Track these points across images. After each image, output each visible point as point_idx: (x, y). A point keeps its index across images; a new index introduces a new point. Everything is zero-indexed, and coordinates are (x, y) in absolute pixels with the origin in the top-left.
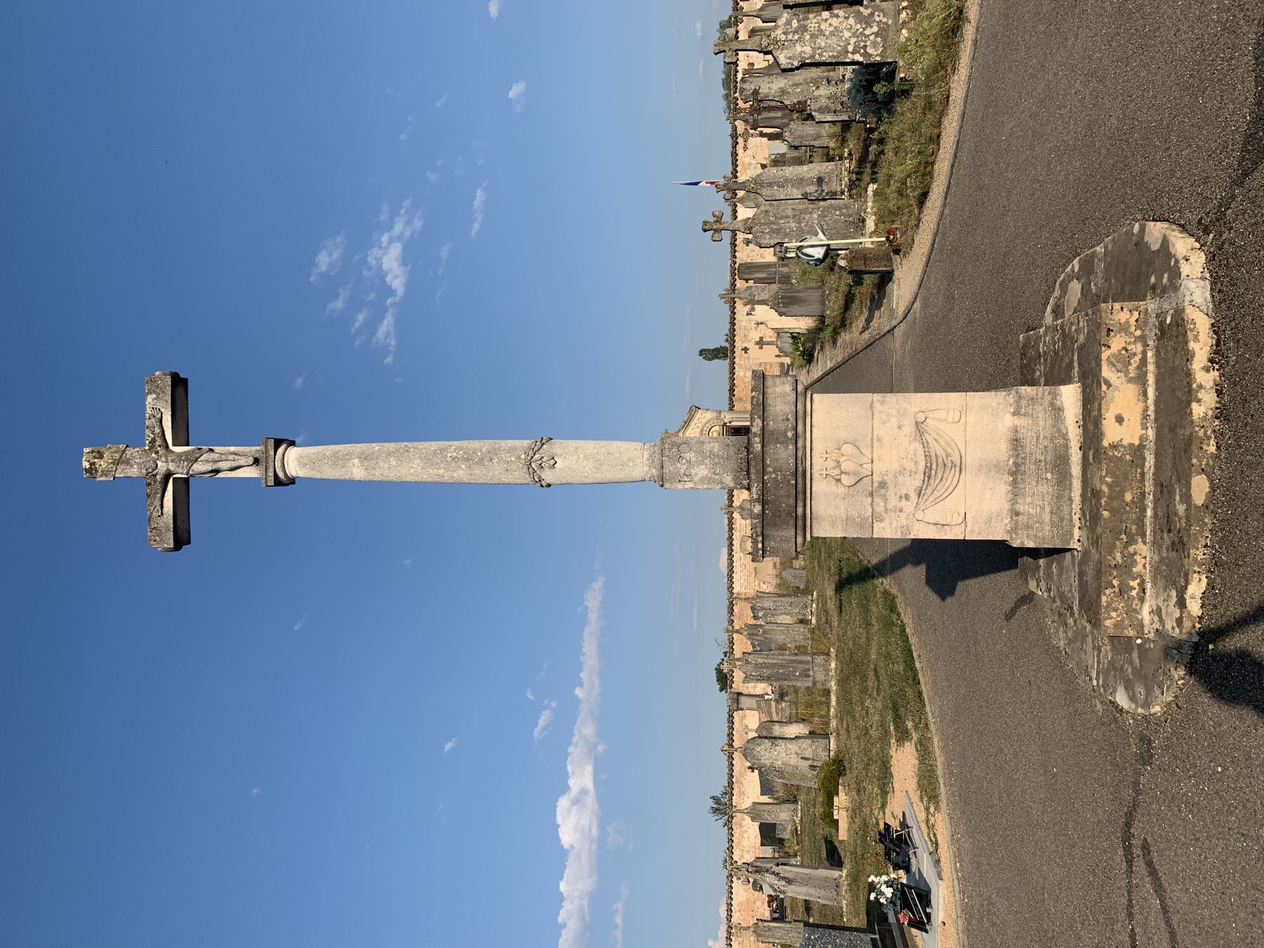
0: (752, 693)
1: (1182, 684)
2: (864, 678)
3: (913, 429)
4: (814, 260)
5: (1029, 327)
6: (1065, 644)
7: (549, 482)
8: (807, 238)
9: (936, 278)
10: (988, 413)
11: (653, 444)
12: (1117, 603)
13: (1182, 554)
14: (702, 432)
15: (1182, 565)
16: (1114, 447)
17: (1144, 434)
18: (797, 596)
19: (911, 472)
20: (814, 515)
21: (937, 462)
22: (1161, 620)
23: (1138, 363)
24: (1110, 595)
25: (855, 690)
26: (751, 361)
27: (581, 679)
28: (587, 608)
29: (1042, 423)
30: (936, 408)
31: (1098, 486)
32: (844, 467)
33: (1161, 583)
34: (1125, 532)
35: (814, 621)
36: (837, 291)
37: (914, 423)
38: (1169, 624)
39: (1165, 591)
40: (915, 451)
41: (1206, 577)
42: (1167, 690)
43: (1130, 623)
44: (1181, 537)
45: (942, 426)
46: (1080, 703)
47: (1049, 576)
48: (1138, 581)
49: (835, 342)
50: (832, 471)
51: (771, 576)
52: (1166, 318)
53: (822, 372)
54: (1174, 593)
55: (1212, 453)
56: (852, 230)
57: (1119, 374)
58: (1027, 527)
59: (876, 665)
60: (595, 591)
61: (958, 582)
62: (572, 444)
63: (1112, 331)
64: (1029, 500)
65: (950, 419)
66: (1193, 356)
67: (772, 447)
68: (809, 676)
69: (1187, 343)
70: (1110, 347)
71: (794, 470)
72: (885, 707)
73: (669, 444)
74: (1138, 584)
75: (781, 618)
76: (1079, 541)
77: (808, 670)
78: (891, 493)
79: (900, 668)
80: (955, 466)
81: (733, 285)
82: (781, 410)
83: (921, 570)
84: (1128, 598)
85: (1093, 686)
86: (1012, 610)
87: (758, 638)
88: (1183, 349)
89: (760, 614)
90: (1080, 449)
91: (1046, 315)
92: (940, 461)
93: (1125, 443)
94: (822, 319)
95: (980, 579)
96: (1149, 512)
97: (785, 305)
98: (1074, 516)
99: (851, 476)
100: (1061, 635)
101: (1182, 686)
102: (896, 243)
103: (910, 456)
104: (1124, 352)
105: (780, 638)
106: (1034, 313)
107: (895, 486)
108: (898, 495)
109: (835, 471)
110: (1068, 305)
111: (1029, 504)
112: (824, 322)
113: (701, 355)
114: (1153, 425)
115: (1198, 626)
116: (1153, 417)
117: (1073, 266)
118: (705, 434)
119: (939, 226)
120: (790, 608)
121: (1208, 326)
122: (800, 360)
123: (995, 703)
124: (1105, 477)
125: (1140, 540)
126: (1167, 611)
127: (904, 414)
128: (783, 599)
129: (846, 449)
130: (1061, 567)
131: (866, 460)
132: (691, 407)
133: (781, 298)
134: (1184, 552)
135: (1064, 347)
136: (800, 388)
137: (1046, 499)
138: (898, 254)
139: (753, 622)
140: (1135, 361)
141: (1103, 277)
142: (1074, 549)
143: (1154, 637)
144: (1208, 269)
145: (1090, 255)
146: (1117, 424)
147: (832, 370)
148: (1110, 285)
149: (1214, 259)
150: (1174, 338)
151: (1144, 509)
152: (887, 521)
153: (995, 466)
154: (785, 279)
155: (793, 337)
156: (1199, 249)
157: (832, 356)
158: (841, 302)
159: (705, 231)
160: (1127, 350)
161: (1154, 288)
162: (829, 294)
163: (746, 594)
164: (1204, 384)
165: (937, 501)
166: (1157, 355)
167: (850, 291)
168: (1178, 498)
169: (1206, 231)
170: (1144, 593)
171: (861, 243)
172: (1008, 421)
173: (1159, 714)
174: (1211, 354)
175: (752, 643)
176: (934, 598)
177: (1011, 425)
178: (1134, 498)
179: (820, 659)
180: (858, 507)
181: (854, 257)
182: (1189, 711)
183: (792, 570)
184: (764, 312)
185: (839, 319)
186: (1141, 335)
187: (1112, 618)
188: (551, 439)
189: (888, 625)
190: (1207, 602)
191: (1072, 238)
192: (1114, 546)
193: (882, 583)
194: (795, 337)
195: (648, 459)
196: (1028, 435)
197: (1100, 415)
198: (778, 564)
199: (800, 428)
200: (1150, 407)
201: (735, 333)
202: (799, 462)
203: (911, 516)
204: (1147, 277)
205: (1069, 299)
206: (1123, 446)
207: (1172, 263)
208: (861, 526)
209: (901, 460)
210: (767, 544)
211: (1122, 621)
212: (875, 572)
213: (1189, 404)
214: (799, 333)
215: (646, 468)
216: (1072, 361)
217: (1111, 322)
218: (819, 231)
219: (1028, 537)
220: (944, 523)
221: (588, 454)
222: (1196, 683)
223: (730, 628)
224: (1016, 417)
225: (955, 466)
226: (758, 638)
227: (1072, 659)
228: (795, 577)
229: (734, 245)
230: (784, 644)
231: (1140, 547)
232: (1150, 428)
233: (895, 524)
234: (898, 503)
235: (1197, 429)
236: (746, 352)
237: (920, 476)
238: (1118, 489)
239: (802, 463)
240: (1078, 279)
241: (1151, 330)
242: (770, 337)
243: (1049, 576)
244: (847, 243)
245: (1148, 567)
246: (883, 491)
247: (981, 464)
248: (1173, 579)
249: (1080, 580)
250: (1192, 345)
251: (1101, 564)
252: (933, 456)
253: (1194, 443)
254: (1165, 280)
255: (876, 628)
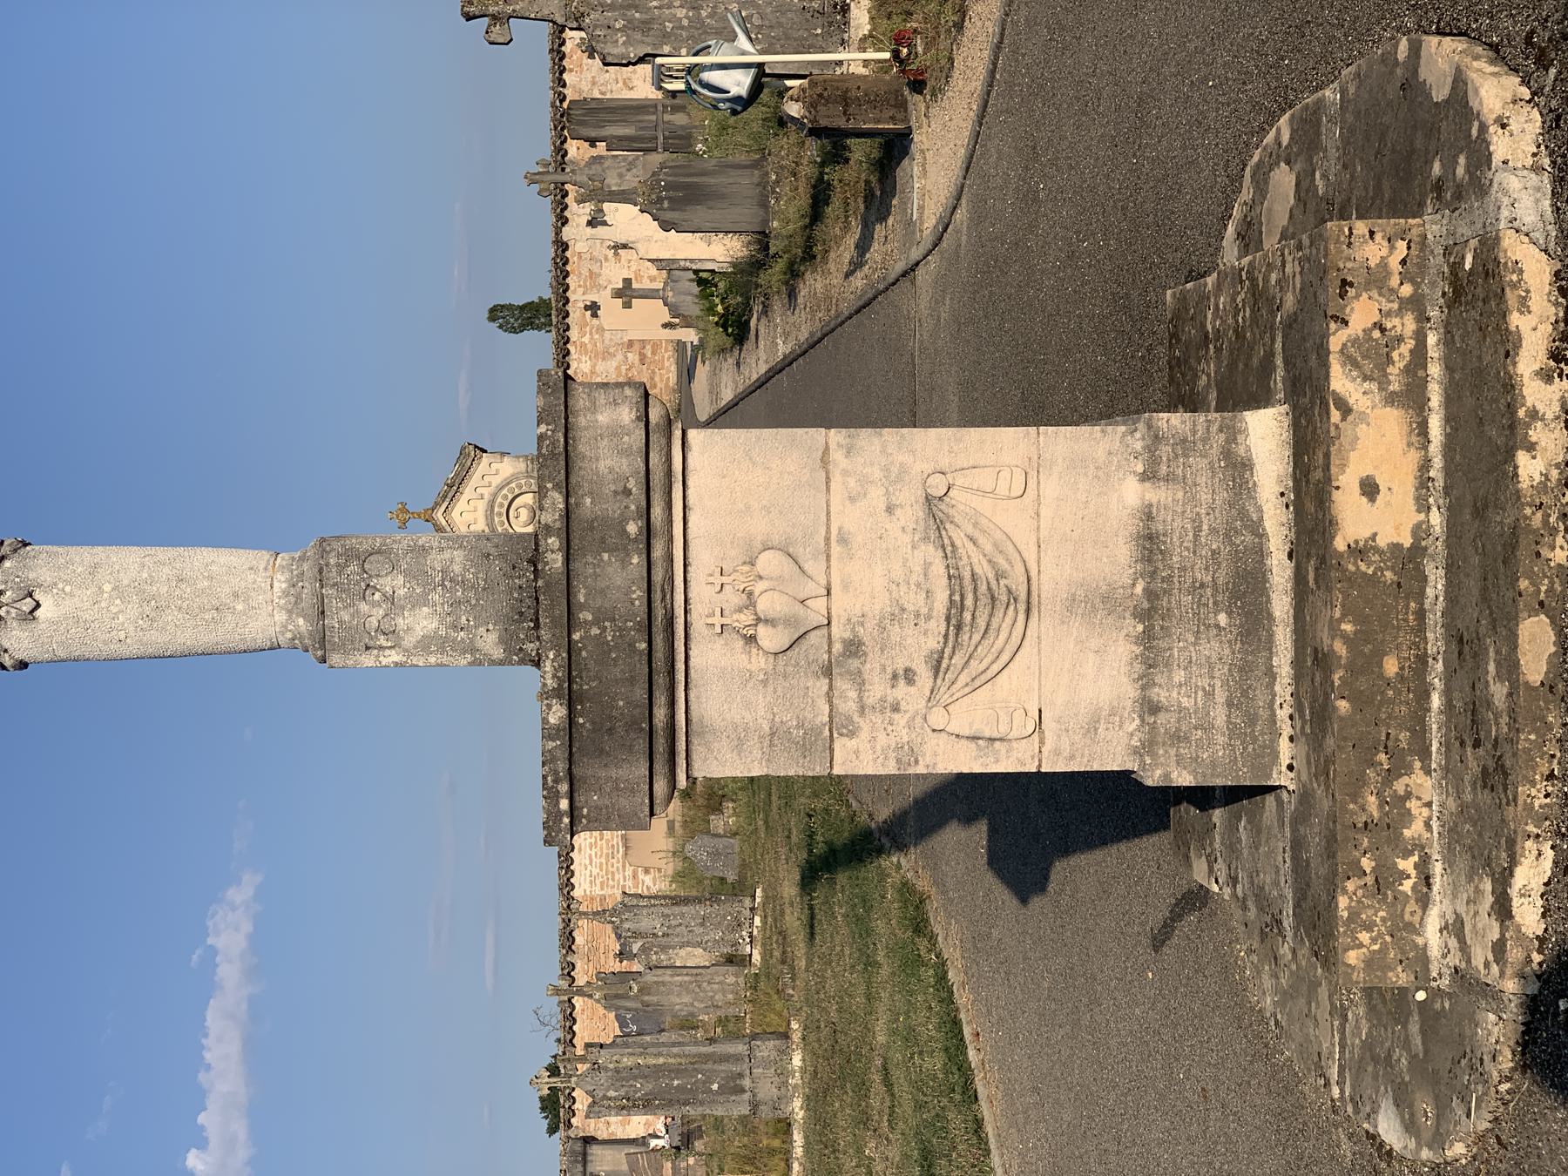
0: (620, 1135)
1: (1508, 1092)
2: (863, 1089)
3: (921, 514)
4: (729, 100)
5: (1191, 271)
6: (1275, 1003)
7: (20, 656)
8: (710, 47)
9: (999, 152)
10: (1086, 474)
11: (297, 555)
12: (1370, 912)
13: (1502, 796)
14: (492, 507)
15: (1503, 821)
16: (1359, 551)
17: (1423, 522)
18: (718, 901)
19: (918, 615)
20: (694, 727)
21: (975, 590)
22: (1464, 948)
23: (1408, 359)
24: (1355, 894)
25: (844, 1117)
26: (607, 335)
27: (202, 1128)
28: (213, 951)
29: (1205, 497)
30: (971, 463)
31: (1327, 641)
32: (764, 605)
33: (1462, 863)
34: (1386, 747)
35: (757, 958)
36: (795, 175)
37: (922, 500)
38: (1481, 954)
39: (1470, 880)
40: (927, 566)
41: (1553, 847)
42: (1478, 1107)
43: (1399, 957)
44: (1501, 757)
45: (984, 505)
46: (1307, 1140)
47: (1232, 848)
48: (1416, 858)
49: (792, 295)
50: (735, 617)
51: (663, 855)
52: (1463, 258)
53: (768, 366)
54: (1488, 886)
55: (1559, 565)
56: (819, 31)
57: (1366, 385)
58: (1178, 738)
59: (885, 1059)
60: (234, 909)
61: (1051, 864)
62: (83, 556)
63: (1351, 285)
64: (1179, 676)
65: (1002, 489)
66: (1518, 345)
67: (590, 559)
68: (743, 1091)
69: (1505, 316)
70: (1346, 323)
71: (646, 616)
72: (906, 1156)
73: (339, 555)
74: (1416, 866)
75: (682, 952)
76: (1290, 768)
77: (741, 1076)
78: (872, 667)
79: (935, 1063)
80: (1015, 600)
81: (560, 151)
82: (611, 470)
83: (979, 834)
84: (1395, 898)
85: (1333, 1100)
86: (1165, 925)
87: (629, 1004)
88: (1498, 329)
89: (636, 948)
90: (1290, 556)
91: (1224, 243)
92: (983, 588)
93: (1382, 542)
94: (762, 238)
95: (1098, 854)
96: (1436, 701)
97: (676, 204)
98: (1278, 712)
99: (780, 628)
100: (1268, 982)
101: (1508, 1097)
102: (912, 67)
103: (913, 580)
104: (1376, 334)
105: (680, 1002)
106: (1202, 240)
107: (882, 651)
108: (889, 670)
109: (742, 617)
110: (1269, 221)
111: (1180, 685)
112: (767, 248)
113: (492, 318)
114: (1441, 501)
115: (1537, 958)
116: (1440, 484)
117: (1279, 130)
118: (500, 514)
119: (1003, 29)
120: (701, 930)
121: (1547, 277)
122: (718, 337)
123: (1134, 1144)
124: (1340, 621)
125: (1418, 764)
126: (1474, 926)
127: (899, 479)
128: (685, 909)
129: (769, 562)
130: (1256, 829)
131: (813, 588)
132: (463, 448)
133: (665, 188)
134: (1506, 795)
135: (1255, 319)
136: (655, 415)
137: (1217, 674)
138: (921, 93)
139: (616, 966)
140: (1401, 355)
141: (1339, 158)
142: (1280, 787)
143: (1450, 986)
144: (1547, 147)
145: (1311, 105)
146: (1364, 499)
147: (789, 362)
148: (1352, 176)
149: (1558, 126)
150: (1480, 304)
151: (1425, 695)
152: (864, 734)
153: (1105, 599)
154: (680, 142)
155: (701, 282)
156: (1529, 102)
157: (787, 329)
158: (804, 200)
159: (469, 17)
160: (1383, 330)
161: (1438, 187)
162: (777, 182)
163: (603, 898)
164: (1540, 408)
165: (977, 683)
166: (1447, 341)
167: (822, 174)
168: (1492, 667)
169: (1543, 62)
170: (1429, 885)
171: (840, 63)
172: (1132, 493)
173: (1464, 1161)
174: (1554, 341)
175: (617, 1017)
176: (1003, 896)
177: (1139, 502)
178: (1402, 668)
179: (766, 1049)
180: (796, 702)
181: (820, 95)
182: (1521, 1153)
183: (706, 838)
184: (626, 219)
185: (799, 240)
186: (1412, 296)
187: (1361, 946)
188: (26, 545)
189: (911, 963)
190: (1554, 904)
191: (1277, 66)
192: (1361, 781)
193: (899, 866)
194: (705, 281)
195: (286, 594)
196: (1174, 525)
197: (1328, 479)
198: (677, 825)
199: (657, 512)
200: (1436, 460)
201: (568, 268)
202: (657, 596)
203: (919, 720)
204: (1426, 162)
205: (1270, 210)
206: (1376, 550)
207: (1474, 132)
208: (805, 748)
209: (894, 587)
210: (580, 799)
211: (1384, 950)
212: (884, 840)
213: (1510, 456)
214: (713, 271)
215: (280, 617)
216: (1271, 354)
217: (1349, 265)
218: (738, 30)
219: (1178, 764)
220: (995, 735)
221: (126, 582)
222: (1535, 1089)
223: (564, 984)
224: (1147, 484)
225: (1015, 600)
226: (629, 1004)
227: (1290, 1037)
228: (715, 855)
229: (558, 55)
230: (692, 1015)
231: (1419, 781)
232: (1435, 509)
233: (882, 740)
234: (889, 691)
235: (1528, 511)
236: (595, 315)
237: (938, 626)
238: (1367, 649)
239: (664, 597)
240: (1288, 163)
241: (1433, 284)
242: (652, 279)
243: (1232, 848)
244: (809, 62)
245: (1435, 824)
246: (854, 663)
247: (1074, 595)
248: (1486, 852)
249: (1295, 858)
250: (1515, 319)
251: (1334, 822)
252: (967, 575)
253: (1523, 541)
254: (1460, 171)
255: (885, 971)
